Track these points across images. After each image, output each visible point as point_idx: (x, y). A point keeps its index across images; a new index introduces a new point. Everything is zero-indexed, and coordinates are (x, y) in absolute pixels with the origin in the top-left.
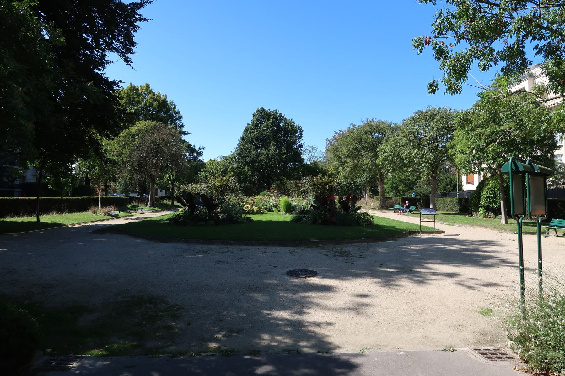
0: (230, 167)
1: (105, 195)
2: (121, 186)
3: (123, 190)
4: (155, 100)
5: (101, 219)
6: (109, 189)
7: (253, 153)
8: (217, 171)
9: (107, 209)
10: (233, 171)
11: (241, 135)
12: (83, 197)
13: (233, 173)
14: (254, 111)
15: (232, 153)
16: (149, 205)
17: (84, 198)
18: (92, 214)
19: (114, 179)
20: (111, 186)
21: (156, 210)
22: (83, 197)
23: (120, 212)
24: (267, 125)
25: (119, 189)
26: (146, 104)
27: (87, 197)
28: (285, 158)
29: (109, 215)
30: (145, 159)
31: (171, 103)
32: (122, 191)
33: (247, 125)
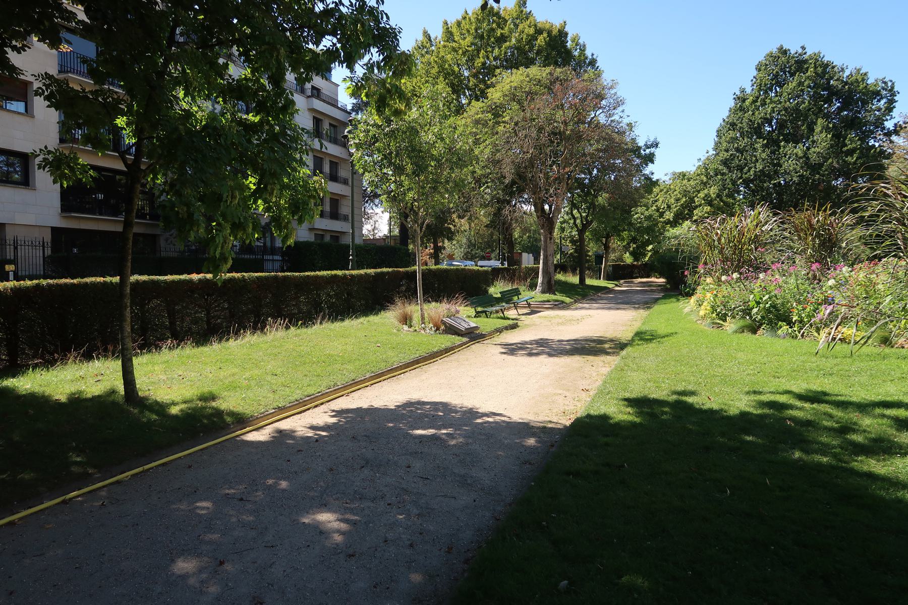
0: (702, 195)
1: (435, 265)
2: (461, 248)
3: (465, 254)
4: (539, 31)
6: (442, 253)
7: (764, 155)
8: (669, 207)
9: (438, 309)
10: (710, 203)
12: (379, 270)
13: (709, 207)
14: (760, 57)
16: (539, 288)
17: (382, 273)
18: (396, 323)
19: (450, 235)
20: (444, 248)
21: (563, 302)
22: (379, 270)
24: (800, 84)
25: (458, 253)
26: (519, 41)
27: (390, 270)
28: (855, 163)
29: (451, 330)
30: (531, 163)
31: (575, 40)
32: (463, 257)
33: (738, 93)
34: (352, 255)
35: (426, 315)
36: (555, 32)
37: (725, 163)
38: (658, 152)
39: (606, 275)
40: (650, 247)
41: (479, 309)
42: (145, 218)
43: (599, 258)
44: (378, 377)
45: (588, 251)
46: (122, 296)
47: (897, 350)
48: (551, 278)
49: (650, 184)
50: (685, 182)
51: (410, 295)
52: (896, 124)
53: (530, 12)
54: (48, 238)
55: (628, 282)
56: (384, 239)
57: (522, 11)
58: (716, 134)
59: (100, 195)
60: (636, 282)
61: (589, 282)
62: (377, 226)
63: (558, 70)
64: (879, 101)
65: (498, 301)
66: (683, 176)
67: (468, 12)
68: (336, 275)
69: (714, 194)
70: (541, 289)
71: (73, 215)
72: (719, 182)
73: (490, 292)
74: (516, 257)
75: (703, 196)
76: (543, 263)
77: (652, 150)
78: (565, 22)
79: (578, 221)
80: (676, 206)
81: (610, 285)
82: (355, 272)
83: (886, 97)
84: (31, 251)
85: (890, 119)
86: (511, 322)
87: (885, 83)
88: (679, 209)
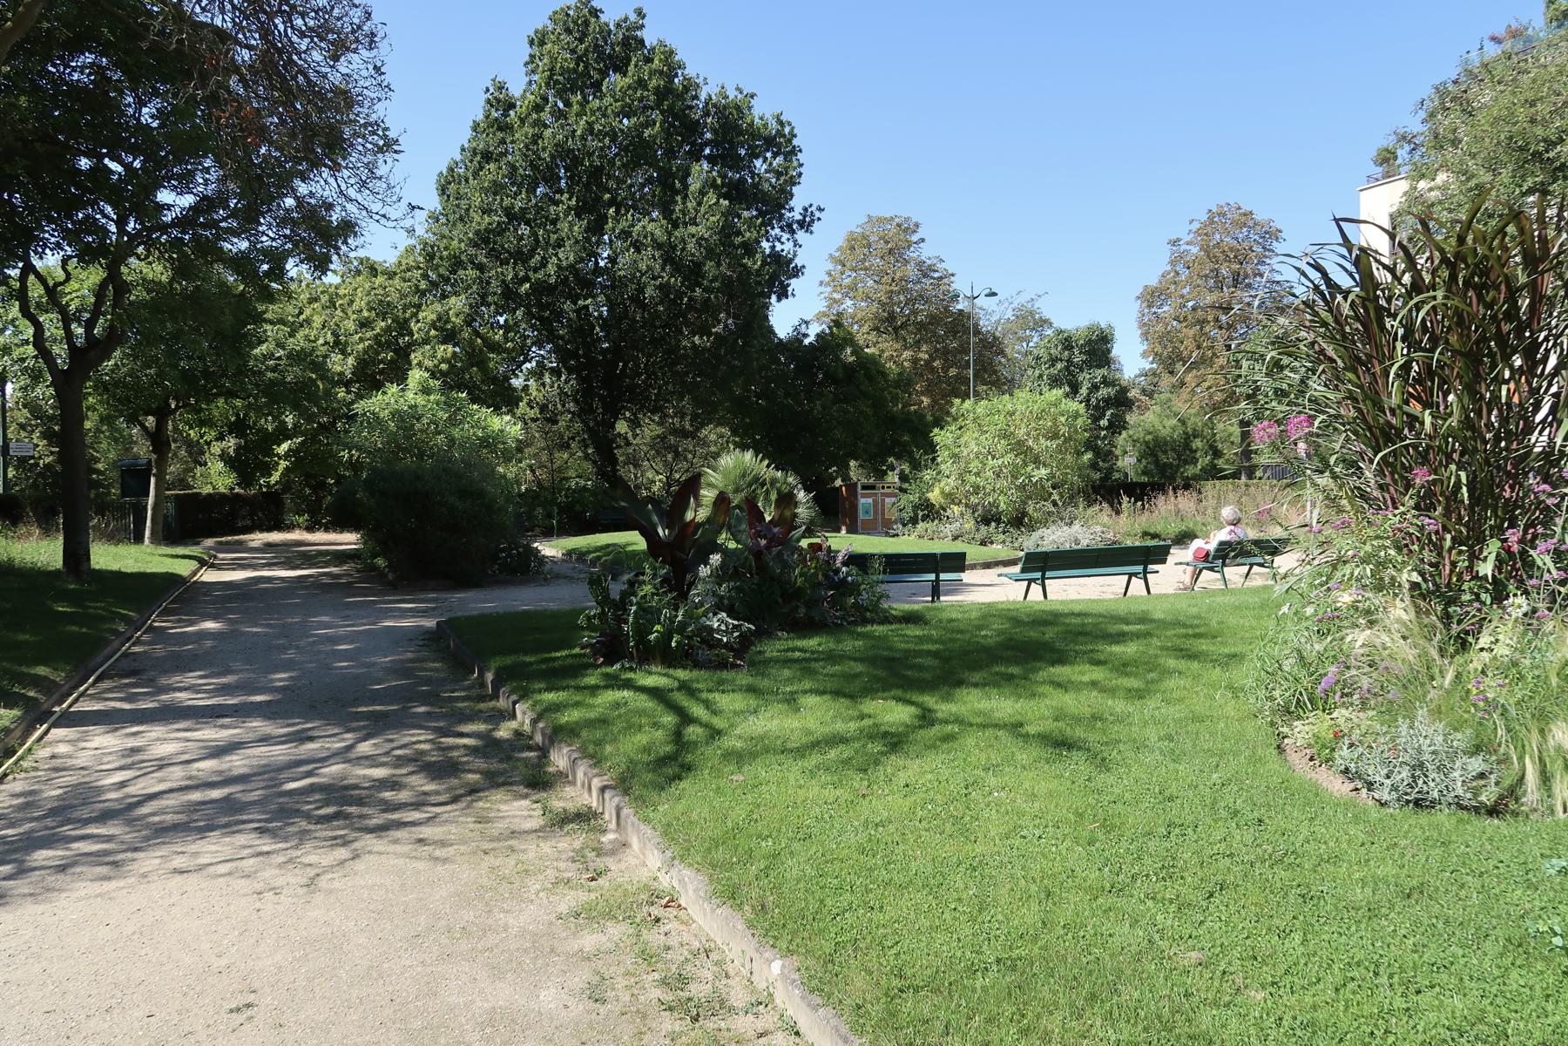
0: (428, 314)
37: (483, 239)
39: (160, 527)
40: (285, 446)
43: (134, 478)
45: (97, 460)
47: (1371, 802)
50: (380, 280)
55: (227, 543)
60: (253, 544)
61: (106, 557)
69: (457, 315)
72: (469, 287)
75: (434, 317)
80: (361, 340)
88: (370, 346)
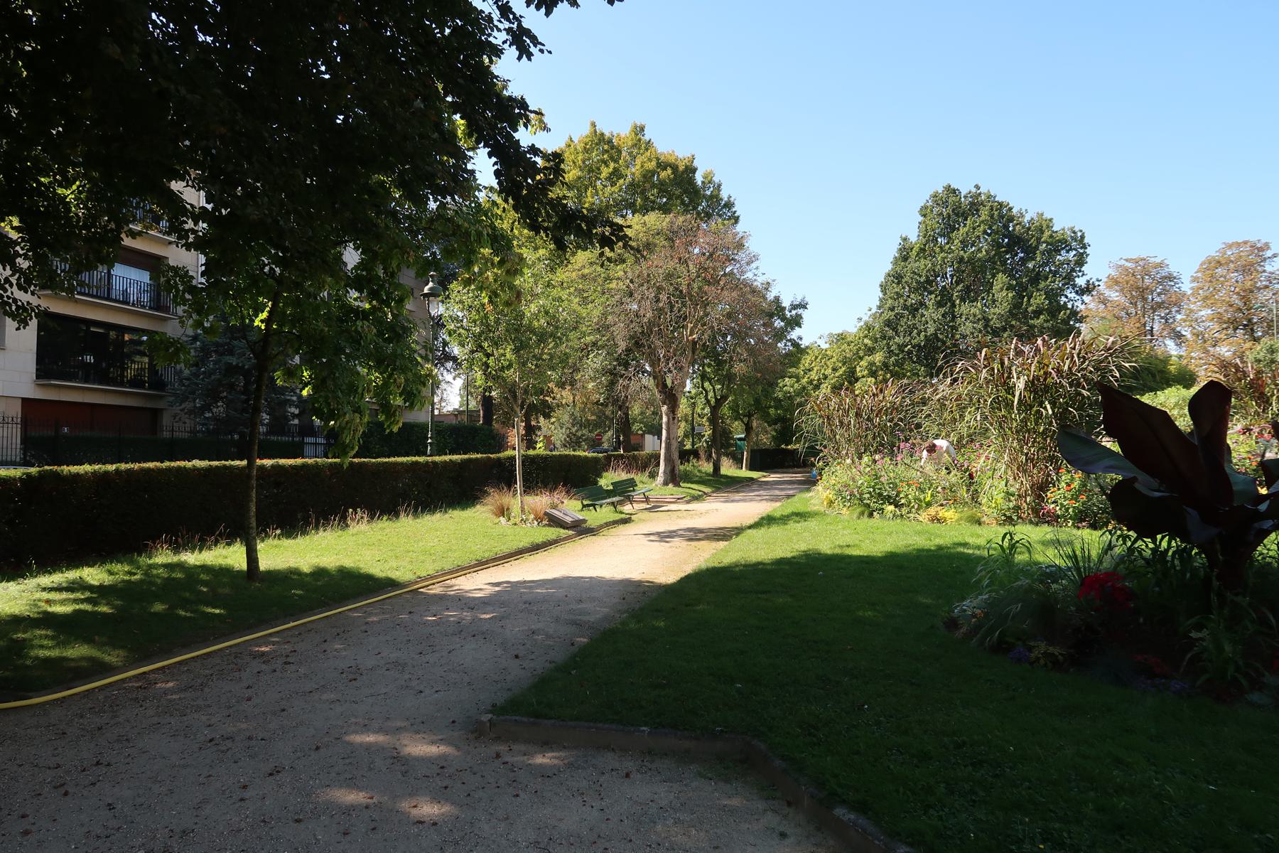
2: (562, 428)
4: (662, 165)
5: (525, 542)
9: (541, 501)
11: (888, 267)
12: (466, 457)
14: (923, 198)
15: (862, 323)
19: (547, 411)
20: (540, 428)
23: (584, 506)
29: (555, 522)
31: (708, 180)
34: (431, 438)
35: (526, 507)
36: (681, 168)
37: (888, 323)
38: (805, 314)
41: (585, 503)
42: (144, 388)
44: (482, 564)
46: (249, 477)
48: (674, 467)
49: (799, 351)
51: (509, 482)
52: (1088, 281)
53: (649, 141)
54: (16, 410)
56: (456, 415)
57: (640, 140)
58: (880, 289)
59: (88, 357)
61: (724, 471)
62: (445, 396)
63: (681, 219)
64: (1068, 252)
65: (609, 494)
66: (841, 338)
67: (573, 139)
68: (417, 463)
70: (662, 479)
71: (52, 382)
73: (600, 484)
74: (633, 440)
76: (666, 447)
77: (800, 311)
78: (693, 156)
79: (711, 394)
81: (755, 475)
82: (437, 459)
83: (1075, 250)
84: (14, 430)
85: (1082, 276)
86: (623, 516)
87: (1074, 232)
